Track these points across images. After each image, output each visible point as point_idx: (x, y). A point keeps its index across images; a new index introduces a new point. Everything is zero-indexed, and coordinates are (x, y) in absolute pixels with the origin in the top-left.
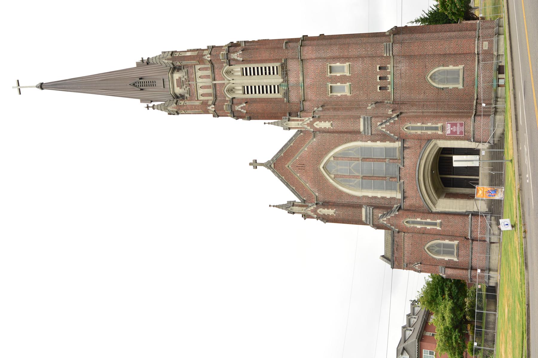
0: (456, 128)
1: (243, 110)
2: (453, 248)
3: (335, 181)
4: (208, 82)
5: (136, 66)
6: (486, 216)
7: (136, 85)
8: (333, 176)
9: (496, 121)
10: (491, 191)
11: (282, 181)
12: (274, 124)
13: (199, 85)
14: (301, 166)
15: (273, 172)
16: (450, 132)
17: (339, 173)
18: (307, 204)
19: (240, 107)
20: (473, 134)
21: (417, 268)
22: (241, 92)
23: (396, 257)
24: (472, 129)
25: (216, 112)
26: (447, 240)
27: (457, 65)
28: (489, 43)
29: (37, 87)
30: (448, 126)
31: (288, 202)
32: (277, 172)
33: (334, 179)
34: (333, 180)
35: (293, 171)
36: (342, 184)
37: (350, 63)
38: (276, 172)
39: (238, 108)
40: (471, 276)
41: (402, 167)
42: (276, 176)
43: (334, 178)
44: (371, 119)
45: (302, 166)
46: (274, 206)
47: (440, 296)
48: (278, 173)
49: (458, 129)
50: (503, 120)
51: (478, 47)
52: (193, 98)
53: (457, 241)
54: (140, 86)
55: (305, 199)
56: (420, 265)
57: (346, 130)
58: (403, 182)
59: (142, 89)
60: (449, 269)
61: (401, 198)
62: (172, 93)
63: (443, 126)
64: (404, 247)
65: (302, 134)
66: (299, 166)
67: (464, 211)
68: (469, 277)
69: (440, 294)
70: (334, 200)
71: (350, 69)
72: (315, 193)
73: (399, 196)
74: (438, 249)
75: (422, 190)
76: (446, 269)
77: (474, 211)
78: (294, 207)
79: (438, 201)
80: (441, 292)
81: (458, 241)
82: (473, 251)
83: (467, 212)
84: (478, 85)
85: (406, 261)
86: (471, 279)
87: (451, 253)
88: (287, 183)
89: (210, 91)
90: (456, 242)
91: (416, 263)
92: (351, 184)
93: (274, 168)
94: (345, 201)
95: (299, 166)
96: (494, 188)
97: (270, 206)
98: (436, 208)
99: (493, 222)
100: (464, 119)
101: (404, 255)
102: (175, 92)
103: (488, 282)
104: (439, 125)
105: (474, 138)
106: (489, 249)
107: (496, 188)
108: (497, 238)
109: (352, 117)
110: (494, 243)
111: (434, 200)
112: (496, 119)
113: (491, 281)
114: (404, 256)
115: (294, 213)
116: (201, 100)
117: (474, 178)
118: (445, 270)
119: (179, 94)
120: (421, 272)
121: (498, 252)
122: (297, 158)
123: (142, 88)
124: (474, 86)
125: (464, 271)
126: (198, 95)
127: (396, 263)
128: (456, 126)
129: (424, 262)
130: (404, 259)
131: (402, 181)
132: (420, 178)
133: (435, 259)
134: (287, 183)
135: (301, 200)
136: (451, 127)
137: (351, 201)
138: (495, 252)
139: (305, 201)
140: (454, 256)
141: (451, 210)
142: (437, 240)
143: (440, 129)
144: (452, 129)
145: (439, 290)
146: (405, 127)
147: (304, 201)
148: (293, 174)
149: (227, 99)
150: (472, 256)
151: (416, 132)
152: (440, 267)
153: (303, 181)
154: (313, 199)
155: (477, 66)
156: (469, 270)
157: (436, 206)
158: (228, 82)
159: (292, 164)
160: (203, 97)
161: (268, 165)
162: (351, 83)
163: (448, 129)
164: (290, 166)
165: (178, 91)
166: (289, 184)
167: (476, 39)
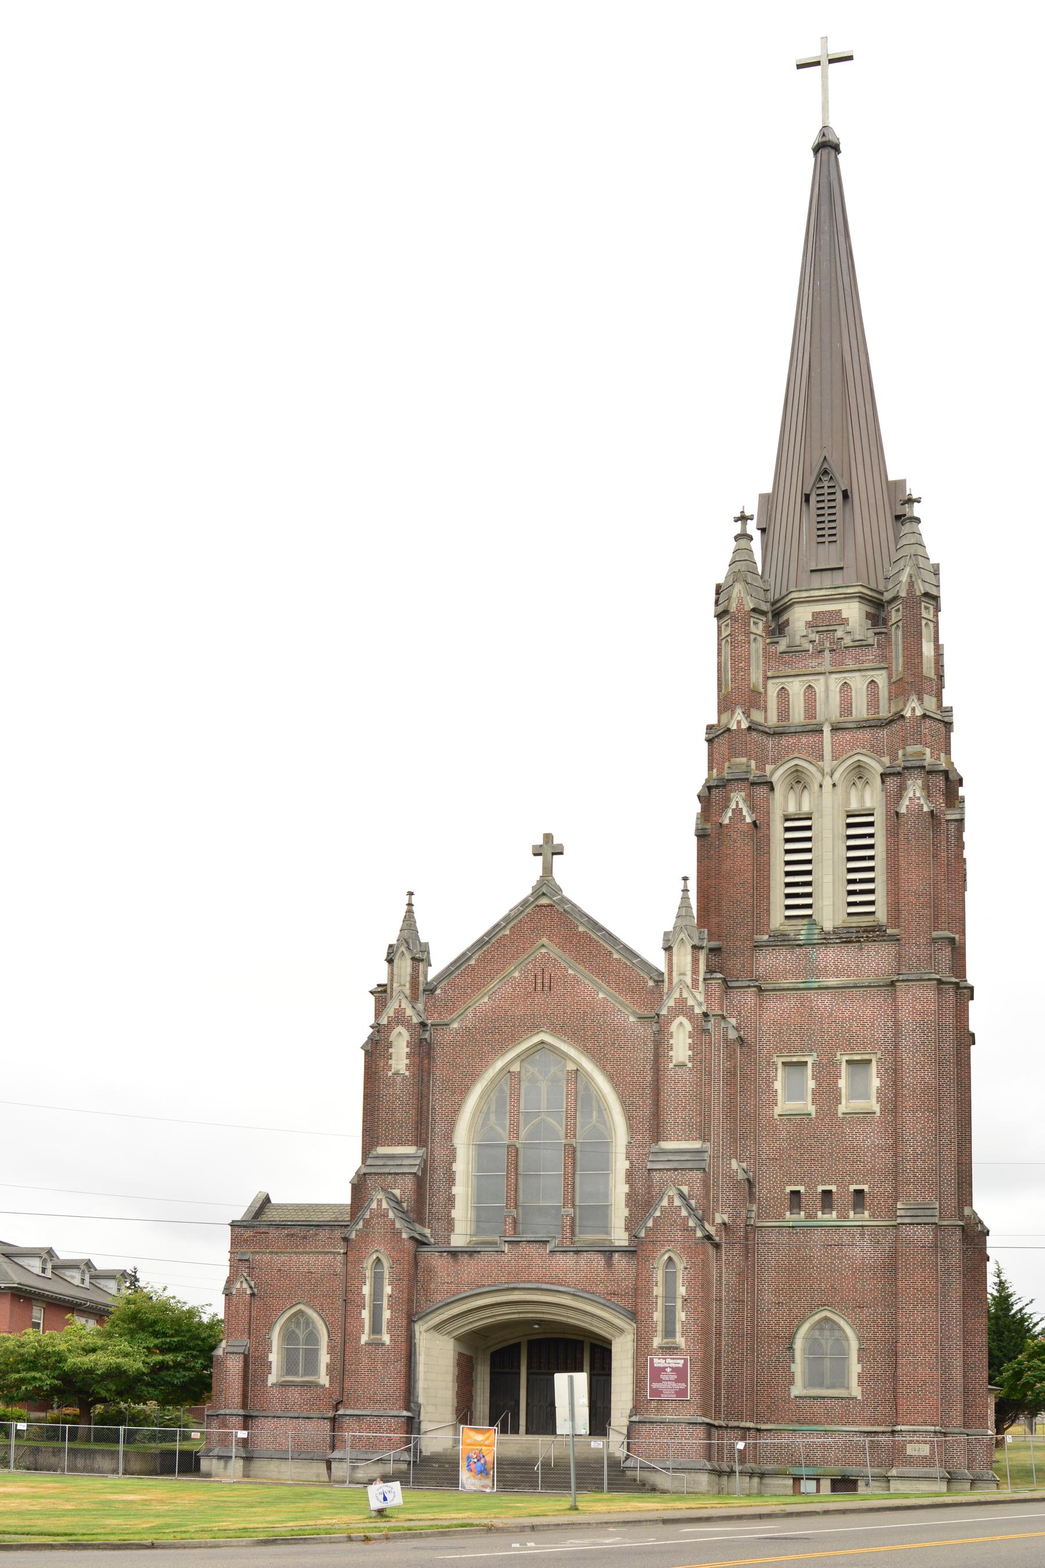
0: (667, 1381)
4: (829, 709)
5: (891, 477)
7: (825, 478)
8: (515, 1068)
9: (693, 1475)
10: (482, 1461)
12: (741, 558)
13: (819, 684)
14: (546, 981)
15: (525, 903)
17: (524, 1085)
18: (422, 998)
20: (652, 1420)
22: (792, 809)
24: (668, 1417)
27: (861, 1383)
28: (925, 1457)
29: (825, 130)
30: (679, 1361)
32: (523, 915)
33: (505, 1072)
34: (502, 1069)
35: (530, 960)
36: (492, 1094)
38: (522, 911)
39: (738, 799)
40: (226, 1415)
41: (549, 1247)
42: (511, 910)
43: (509, 1072)
48: (521, 917)
49: (668, 1386)
54: (820, 491)
55: (438, 991)
64: (301, 1253)
66: (547, 977)
67: (421, 1400)
68: (222, 1412)
70: (438, 1074)
72: (458, 1020)
81: (327, 1386)
85: (257, 1257)
87: (290, 1365)
88: (488, 942)
92: (493, 1117)
93: (537, 906)
94: (438, 1100)
95: (547, 977)
101: (276, 1253)
104: (680, 1340)
105: (639, 1422)
107: (492, 1472)
112: (697, 1475)
116: (765, 687)
119: (787, 621)
120: (226, 1295)
123: (813, 499)
124: (799, 1422)
125: (238, 1400)
127: (249, 1233)
129: (257, 1302)
134: (488, 942)
135: (433, 980)
136: (674, 1369)
139: (433, 994)
143: (667, 1343)
144: (669, 1370)
147: (430, 990)
149: (769, 768)
152: (246, 1341)
154: (440, 1014)
155: (857, 1429)
158: (827, 770)
161: (546, 886)
163: (668, 1361)
164: (543, 950)
165: (800, 617)
166: (485, 948)
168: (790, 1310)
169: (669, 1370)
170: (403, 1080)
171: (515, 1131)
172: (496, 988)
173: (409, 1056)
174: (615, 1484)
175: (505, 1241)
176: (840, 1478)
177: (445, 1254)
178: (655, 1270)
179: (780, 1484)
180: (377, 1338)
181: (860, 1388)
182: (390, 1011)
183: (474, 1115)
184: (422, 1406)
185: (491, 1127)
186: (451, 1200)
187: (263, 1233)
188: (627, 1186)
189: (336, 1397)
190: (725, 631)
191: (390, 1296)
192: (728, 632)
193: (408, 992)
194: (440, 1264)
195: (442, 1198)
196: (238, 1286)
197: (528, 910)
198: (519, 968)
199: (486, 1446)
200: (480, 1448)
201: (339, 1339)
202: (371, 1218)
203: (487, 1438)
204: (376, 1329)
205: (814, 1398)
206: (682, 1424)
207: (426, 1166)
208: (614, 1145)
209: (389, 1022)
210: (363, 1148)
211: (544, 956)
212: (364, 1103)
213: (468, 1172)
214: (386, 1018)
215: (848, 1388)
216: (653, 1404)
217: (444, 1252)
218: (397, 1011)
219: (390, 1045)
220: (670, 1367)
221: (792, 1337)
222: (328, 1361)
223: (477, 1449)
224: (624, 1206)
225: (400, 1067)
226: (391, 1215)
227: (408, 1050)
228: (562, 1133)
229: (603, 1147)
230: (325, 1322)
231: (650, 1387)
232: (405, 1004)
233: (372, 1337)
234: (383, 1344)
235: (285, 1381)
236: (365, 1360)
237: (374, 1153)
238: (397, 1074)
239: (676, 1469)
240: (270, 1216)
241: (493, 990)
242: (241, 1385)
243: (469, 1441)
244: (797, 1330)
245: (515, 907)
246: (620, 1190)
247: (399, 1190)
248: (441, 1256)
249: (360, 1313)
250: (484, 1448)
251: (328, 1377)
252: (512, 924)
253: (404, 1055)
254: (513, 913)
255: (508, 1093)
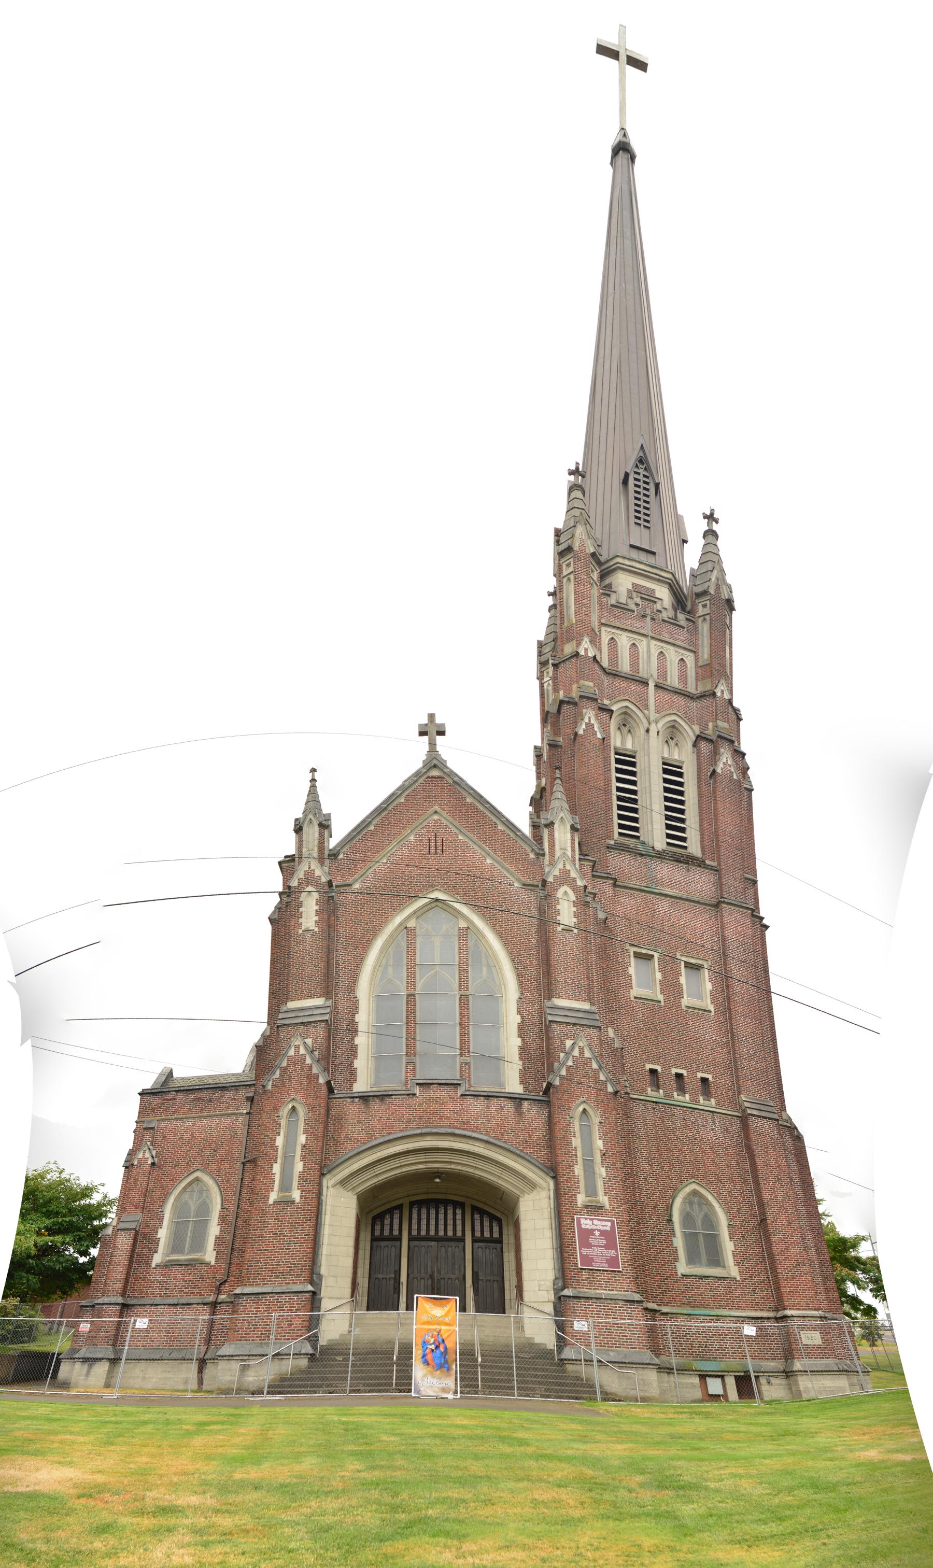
0: (596, 1246)
1: (584, 726)
2: (192, 1250)
3: (396, 929)
6: (308, 1339)
8: (411, 924)
9: (641, 1371)
10: (442, 1349)
11: (390, 796)
14: (438, 844)
15: (418, 774)
16: (587, 1227)
17: (419, 940)
18: (327, 862)
19: (592, 722)
21: (140, 1156)
23: (174, 1099)
24: (604, 1293)
25: (573, 660)
26: (219, 1230)
27: (737, 1263)
28: (819, 1347)
30: (606, 1223)
31: (329, 815)
32: (416, 784)
33: (402, 927)
34: (400, 924)
35: (424, 824)
36: (390, 949)
37: (713, 1014)
38: (416, 781)
40: (103, 1304)
41: (460, 1091)
42: (406, 781)
43: (406, 927)
44: (594, 1027)
45: (440, 848)
46: (313, 780)
47: (48, 1222)
48: (414, 786)
49: (599, 1254)
50: (647, 1394)
51: (804, 1317)
52: (604, 613)
53: (214, 1257)
55: (341, 856)
56: (150, 1162)
57: (553, 962)
58: (414, 1095)
59: (625, 482)
60: (131, 1241)
61: (354, 1091)
62: (619, 560)
63: (601, 1208)
64: (205, 1117)
65: (532, 856)
66: (439, 841)
67: (323, 1271)
68: (100, 1301)
69: (54, 1224)
70: (341, 930)
71: (698, 1009)
72: (360, 881)
73: (360, 1086)
74: (192, 1209)
75: (390, 1145)
76: (132, 1233)
77: (323, 1301)
78: (317, 828)
79: (350, 1193)
80: (61, 1223)
81: (213, 1263)
82: (178, 1307)
83: (320, 1277)
84: (695, 1317)
85: (163, 1125)
86: (93, 1306)
87: (176, 1245)
88: (385, 809)
89: (625, 665)
90: (210, 1256)
91: (154, 1153)
92: (390, 970)
93: (429, 777)
94: (342, 957)
95: (439, 841)
96: (456, 1361)
97: (313, 770)
98: (334, 1186)
99: (288, 1366)
100: (629, 1271)
101: (181, 1119)
102: (619, 571)
103: (74, 1359)
104: (604, 1200)
105: (574, 1297)
106: (180, 1357)
107: (454, 1367)
108: (232, 1382)
109: (590, 987)
110: (200, 1371)
111: (356, 1181)
112: (646, 1371)
113: (78, 1365)
114: (176, 1119)
115: (298, 829)
116: (600, 632)
117: (471, 1289)
118: (128, 1229)
120: (126, 1167)
121: (168, 1387)
122: (460, 837)
124: (689, 1304)
125: (119, 1286)
126: (613, 630)
127: (157, 1101)
128: (607, 1247)
129: (156, 1173)
130: (169, 1120)
131: (417, 1090)
132: (429, 1138)
133: (164, 1201)
134: (385, 809)
135: (335, 847)
136: (603, 1233)
137: (341, 973)
138: (168, 1375)
139: (336, 859)
140: (168, 1255)
141: (326, 1231)
142: (222, 1204)
144: (597, 1233)
145: (67, 1219)
146: (587, 1108)
147: (334, 855)
148: (417, 823)
150: (165, 1305)
151: (578, 1134)
152: (138, 1216)
153: (395, 849)
154: (342, 877)
155: (744, 1314)
156: (121, 1298)
157: (338, 1186)
159: (444, 821)
160: (607, 642)
161: (434, 762)
162: (662, 1004)
163: (596, 1222)
164: (436, 817)
166: (383, 814)
167: (820, 1312)
168: (663, 1180)
169: (597, 1233)
170: (312, 935)
171: (411, 981)
172: (393, 851)
173: (318, 913)
174: (493, 1381)
175: (417, 1084)
176: (742, 1374)
177: (357, 1100)
178: (571, 1120)
179: (687, 1383)
180: (286, 1196)
181: (737, 1267)
182: (300, 874)
183: (375, 968)
184: (324, 1279)
185: (390, 979)
186: (353, 1051)
187: (170, 1100)
188: (520, 1039)
189: (221, 1276)
190: (566, 570)
191: (304, 1146)
192: (571, 569)
193: (316, 855)
194: (351, 1110)
195: (345, 1048)
196: (140, 1156)
197: (421, 781)
198: (414, 832)
199: (447, 1324)
200: (438, 1327)
201: (233, 1208)
202: (288, 1065)
203: (447, 1315)
204: (286, 1186)
205: (700, 1277)
206: (619, 1302)
207: (335, 1011)
208: (504, 999)
209: (299, 884)
210: (269, 1010)
211: (436, 821)
212: (271, 967)
213: (369, 1023)
214: (297, 880)
215: (724, 1267)
216: (585, 1275)
217: (356, 1097)
218: (306, 873)
219: (300, 905)
220: (599, 1230)
221: (670, 1208)
222: (217, 1233)
223: (435, 1330)
224: (517, 1059)
225: (309, 925)
226: (308, 1061)
227: (317, 907)
228: (456, 985)
229: (494, 998)
230: (220, 1189)
231: (581, 1253)
232: (315, 865)
233: (280, 1195)
234: (293, 1202)
235: (170, 1261)
236: (272, 1223)
237: (283, 1008)
238: (307, 930)
239: (622, 1363)
240: (173, 1084)
241: (391, 852)
242: (126, 1267)
243: (425, 1318)
244: (673, 1201)
245: (410, 778)
246: (512, 1044)
247: (311, 1040)
248: (353, 1102)
249: (271, 1168)
250: (443, 1328)
251: (215, 1252)
252: (406, 793)
253: (314, 913)
254: (407, 783)
255: (405, 947)
